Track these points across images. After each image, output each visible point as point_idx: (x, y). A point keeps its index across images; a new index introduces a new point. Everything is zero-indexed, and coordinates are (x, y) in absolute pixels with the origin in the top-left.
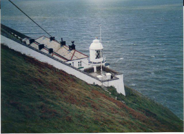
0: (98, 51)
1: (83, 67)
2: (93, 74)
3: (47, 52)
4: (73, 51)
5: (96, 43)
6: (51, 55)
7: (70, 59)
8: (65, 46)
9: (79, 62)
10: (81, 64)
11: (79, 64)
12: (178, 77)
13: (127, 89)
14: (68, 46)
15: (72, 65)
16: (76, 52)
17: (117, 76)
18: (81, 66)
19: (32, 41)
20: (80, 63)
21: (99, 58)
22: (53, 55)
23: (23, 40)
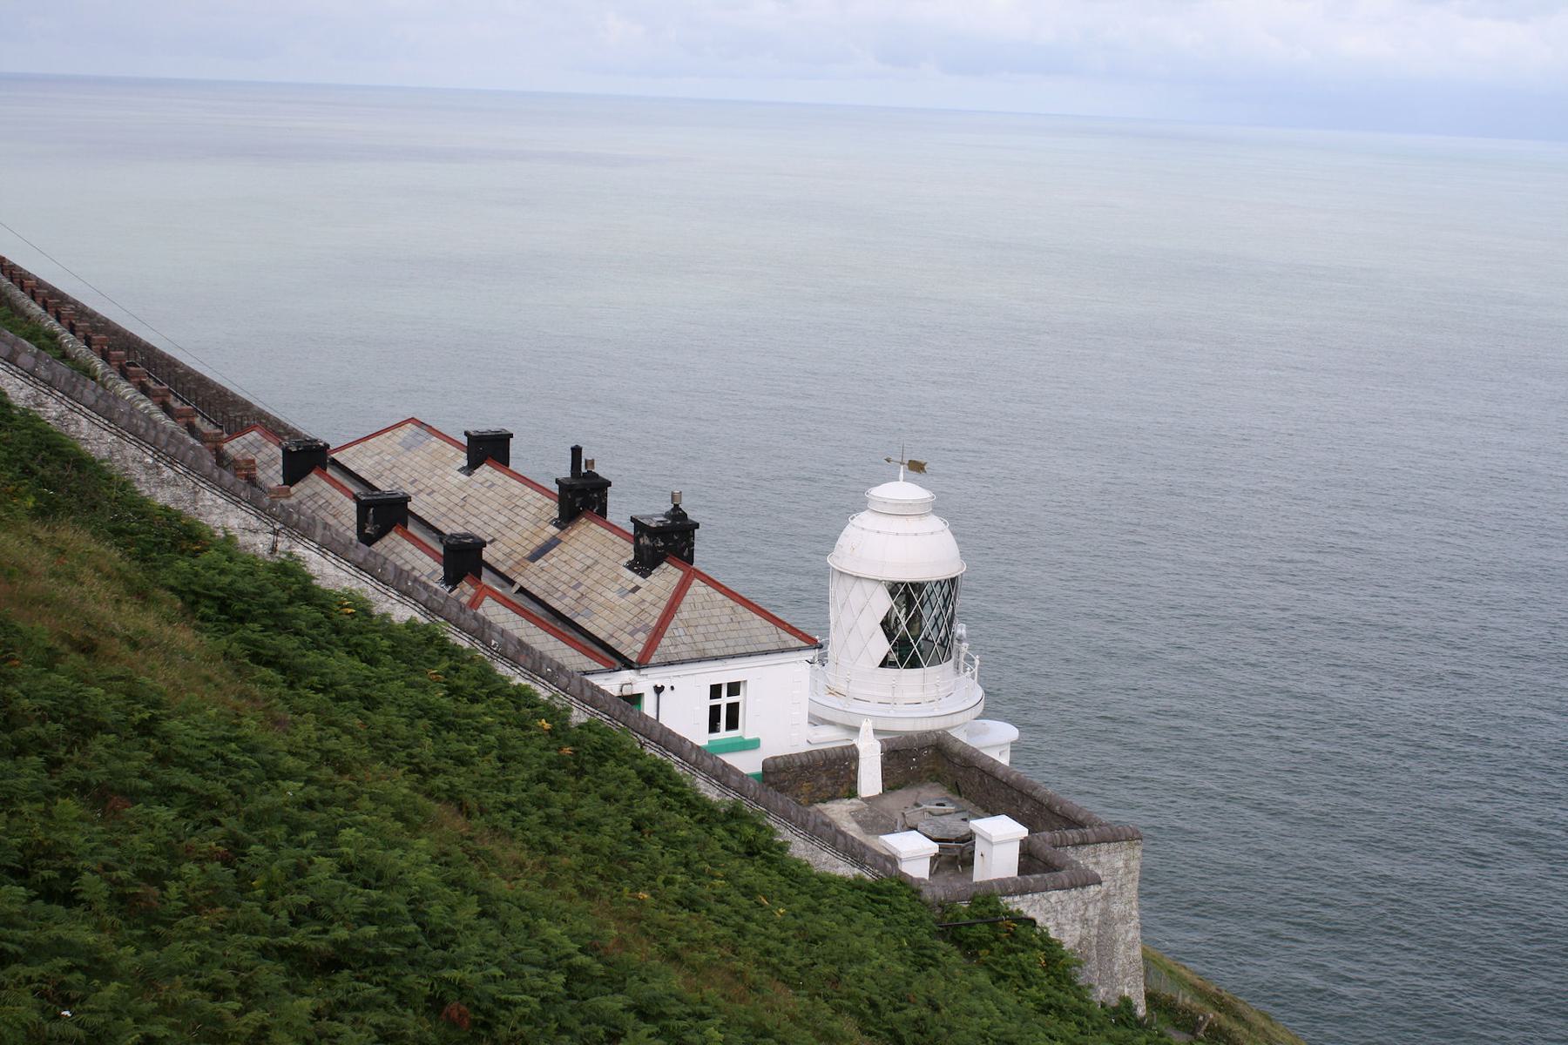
0: (907, 593)
1: (754, 744)
2: (839, 812)
3: (427, 567)
4: (667, 576)
5: (903, 511)
6: (465, 600)
7: (639, 647)
8: (980, 708)
9: (715, 691)
10: (733, 709)
11: (715, 710)
12: (1523, 843)
13: (680, 556)
14: (464, 440)
15: (648, 708)
16: (698, 587)
17: (1084, 858)
18: (733, 723)
19: (307, 458)
20: (724, 701)
21: (914, 664)
22: (475, 603)
23: (235, 448)
